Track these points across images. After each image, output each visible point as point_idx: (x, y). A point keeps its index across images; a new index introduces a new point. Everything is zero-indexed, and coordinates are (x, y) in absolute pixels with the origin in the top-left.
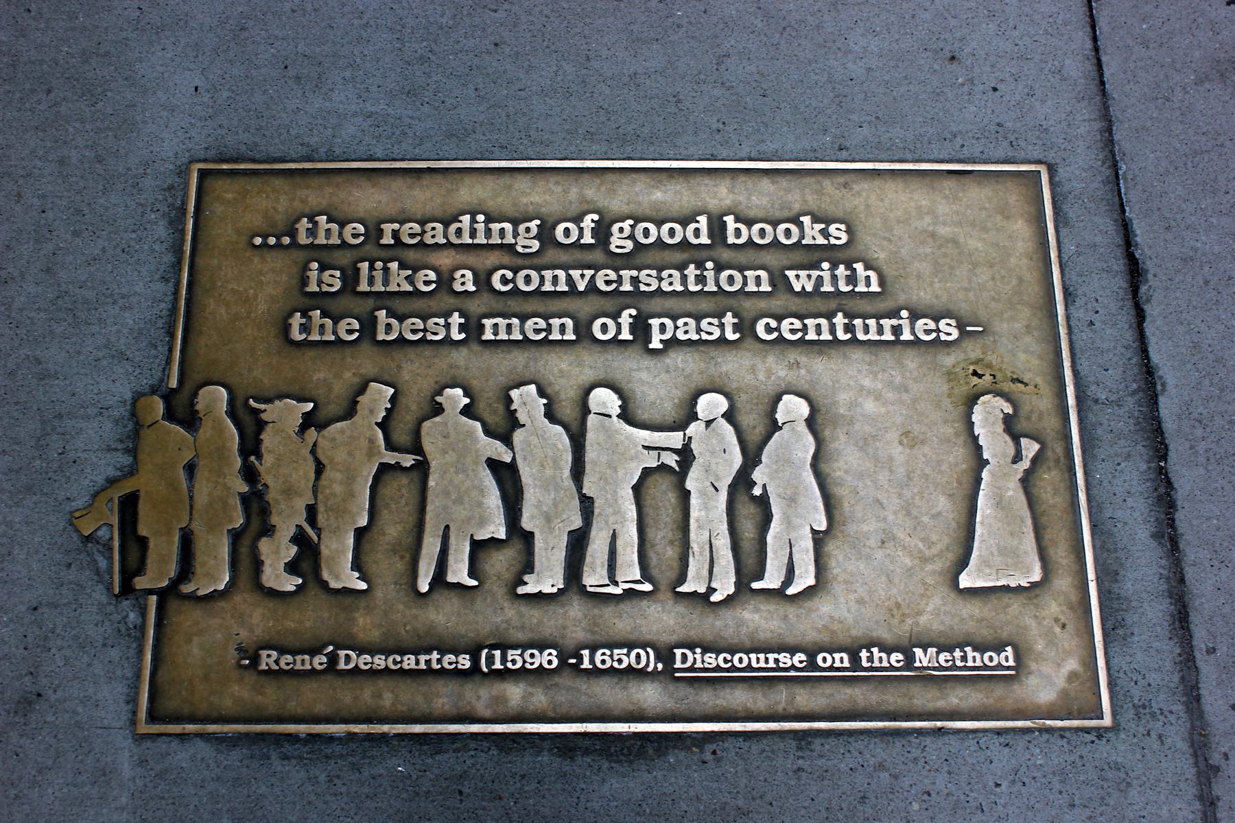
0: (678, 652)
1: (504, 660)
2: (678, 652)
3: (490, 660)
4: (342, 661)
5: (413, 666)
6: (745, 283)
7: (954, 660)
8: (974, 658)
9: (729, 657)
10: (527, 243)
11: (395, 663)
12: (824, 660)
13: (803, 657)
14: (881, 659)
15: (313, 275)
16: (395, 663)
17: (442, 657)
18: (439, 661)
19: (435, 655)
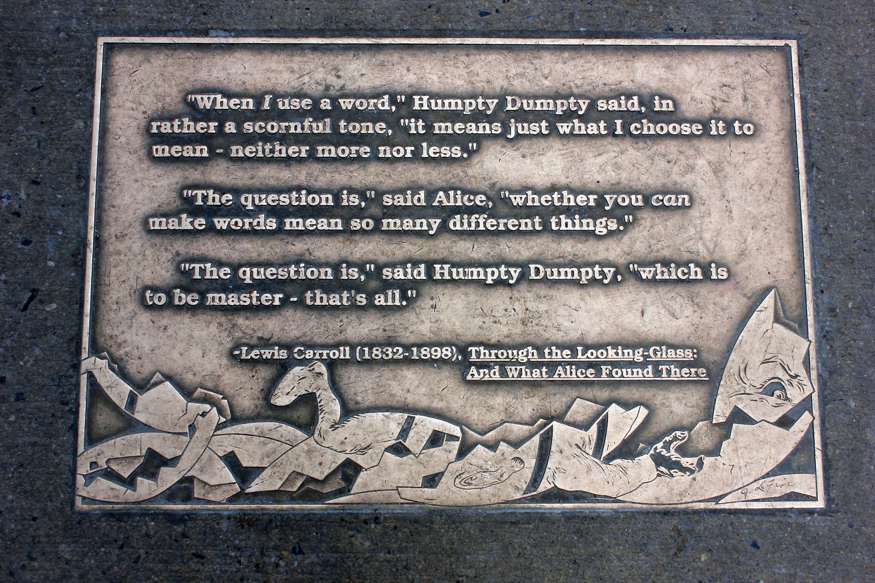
0: (532, 267)
1: (371, 353)
2: (532, 267)
3: (362, 352)
4: (474, 356)
5: (326, 228)
6: (319, 275)
7: (553, 201)
8: (580, 127)
9: (263, 125)
10: (602, 230)
11: (261, 127)
12: (160, 299)
13: (228, 270)
14: (649, 128)
15: (344, 271)
16: (261, 127)
17: (261, 295)
18: (151, 298)
19: (503, 269)
